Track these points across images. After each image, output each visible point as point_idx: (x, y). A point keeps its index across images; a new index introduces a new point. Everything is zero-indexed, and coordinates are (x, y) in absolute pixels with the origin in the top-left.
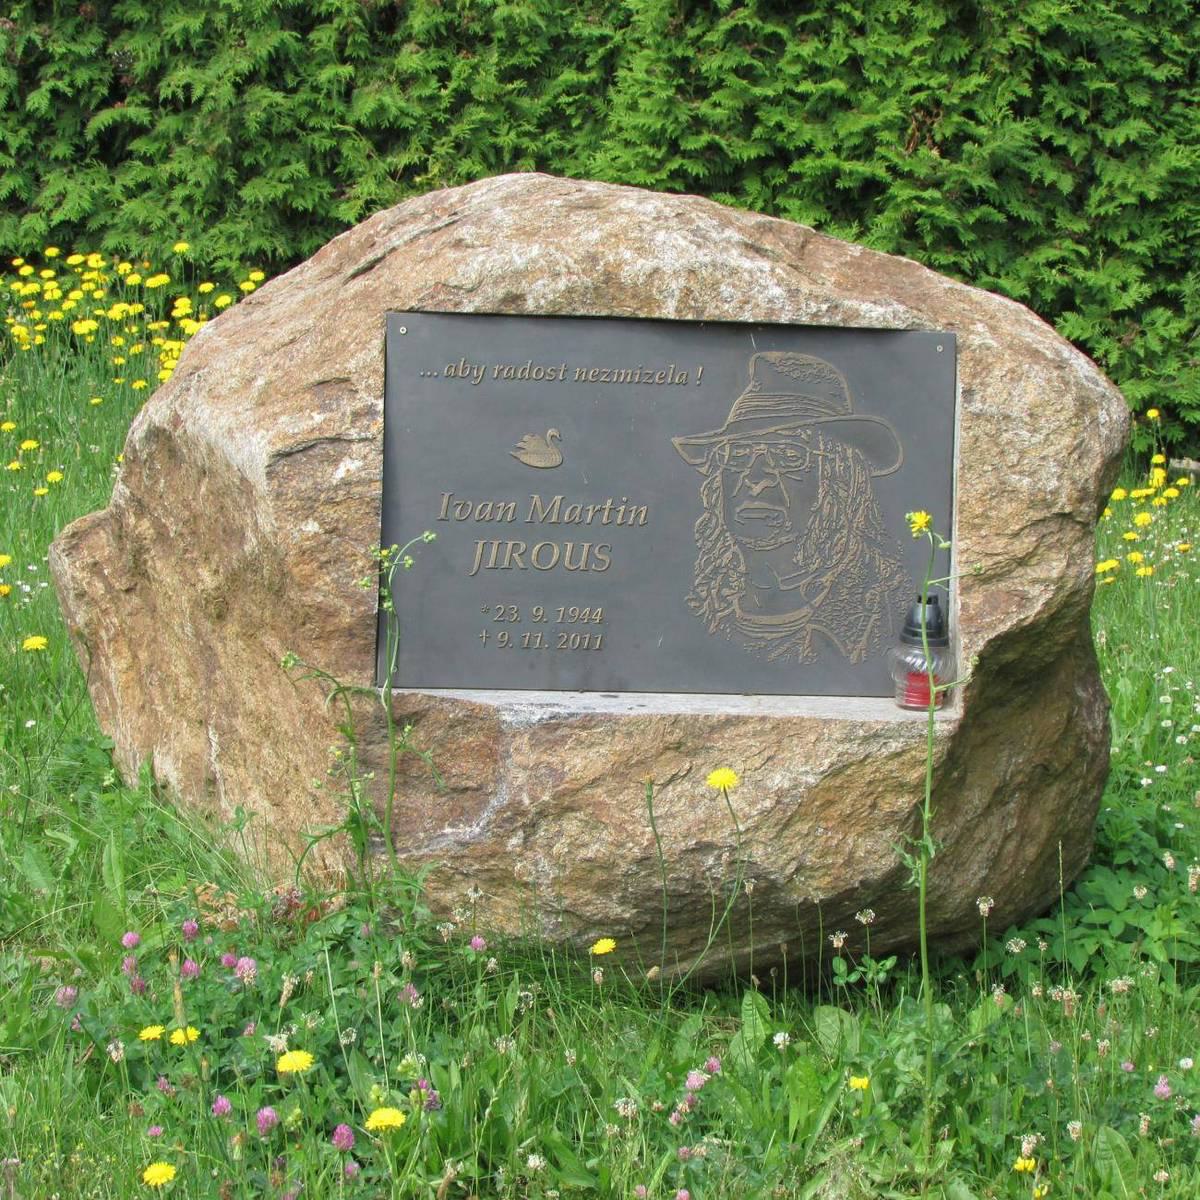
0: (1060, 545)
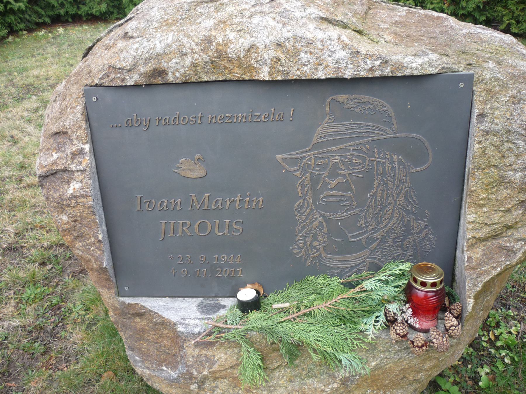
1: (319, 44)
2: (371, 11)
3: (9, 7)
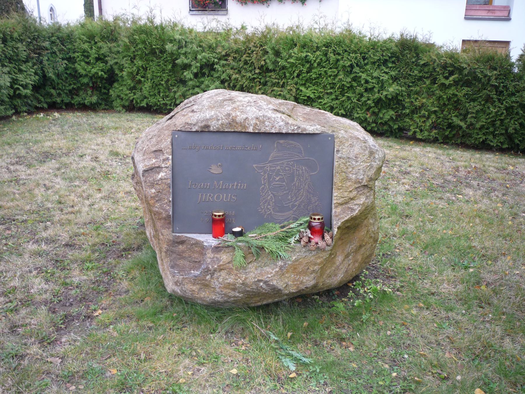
0: (364, 193)
1: (273, 119)
3: (17, 92)
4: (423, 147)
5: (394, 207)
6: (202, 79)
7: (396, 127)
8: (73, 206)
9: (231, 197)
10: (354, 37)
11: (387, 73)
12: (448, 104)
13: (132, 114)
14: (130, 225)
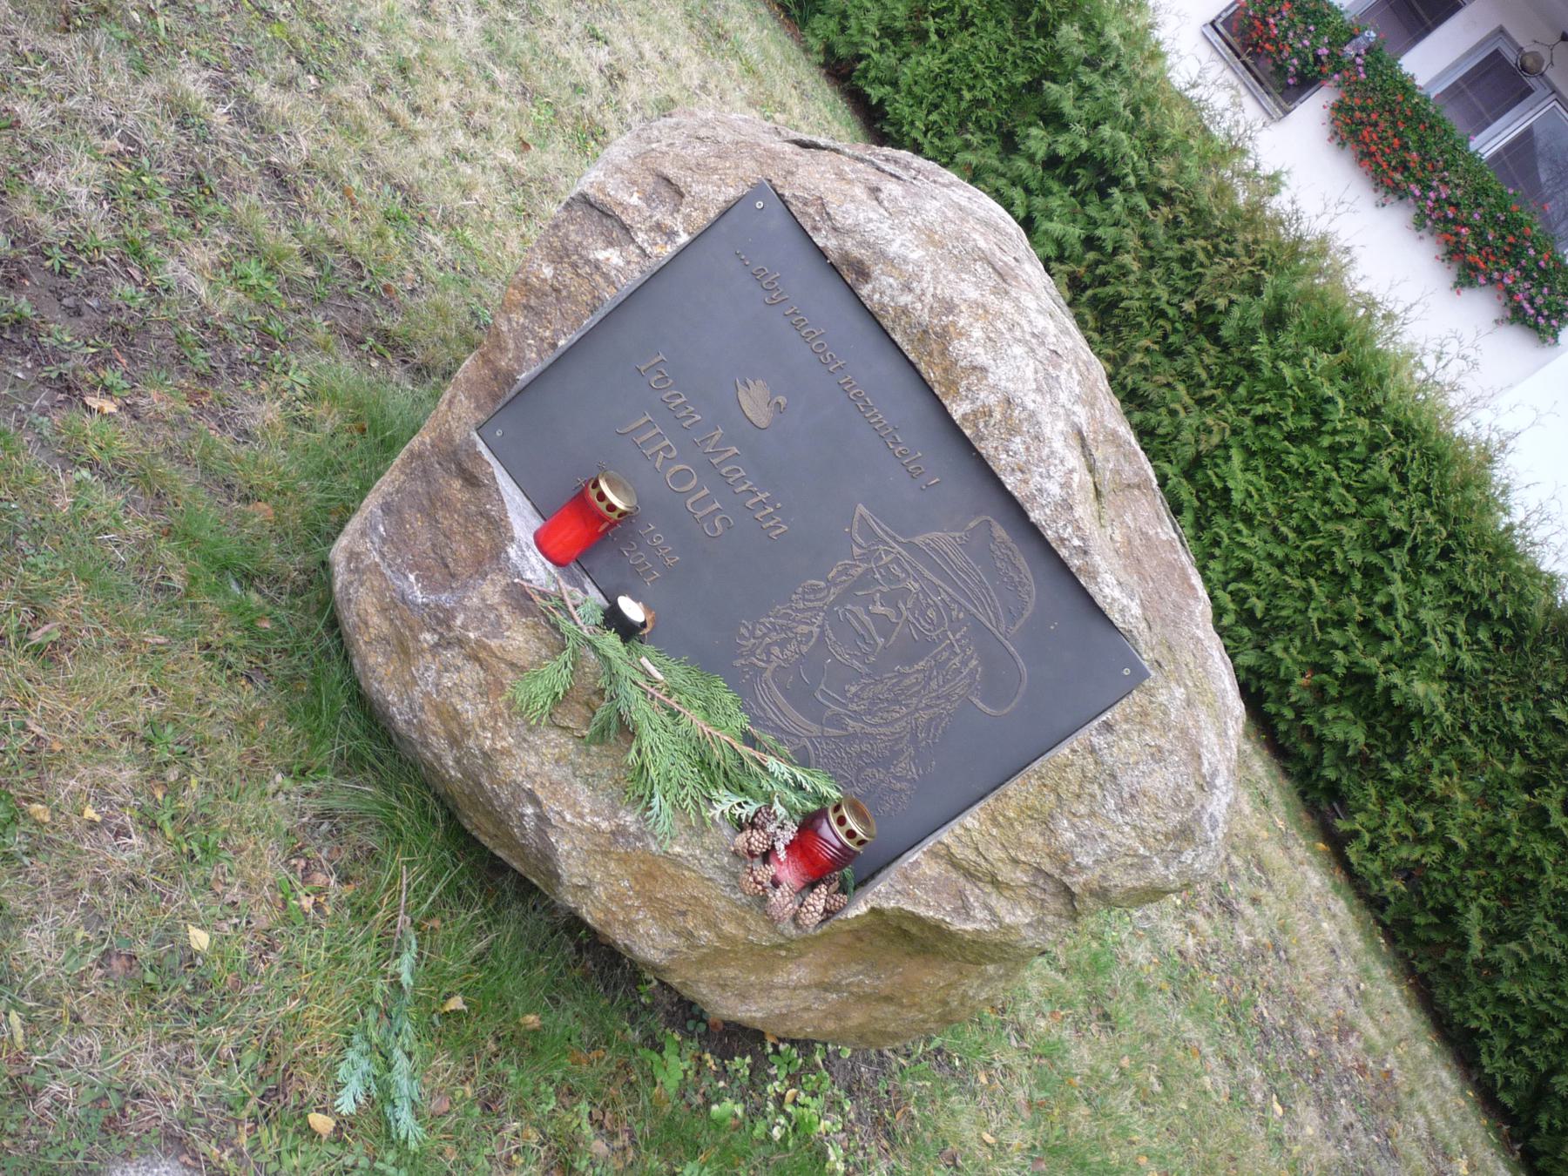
1: (1046, 451)
2: (1136, 492)
4: (1335, 886)
5: (1104, 959)
6: (1055, 187)
7: (1331, 774)
8: (416, 110)
9: (714, 513)
10: (1484, 483)
11: (1453, 641)
12: (1499, 866)
13: (825, 86)
14: (479, 297)
